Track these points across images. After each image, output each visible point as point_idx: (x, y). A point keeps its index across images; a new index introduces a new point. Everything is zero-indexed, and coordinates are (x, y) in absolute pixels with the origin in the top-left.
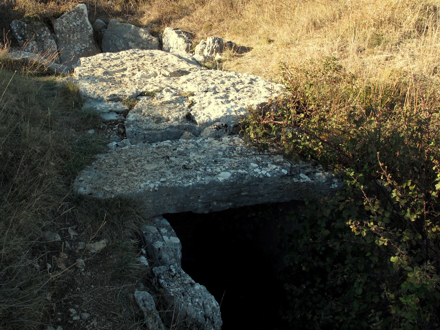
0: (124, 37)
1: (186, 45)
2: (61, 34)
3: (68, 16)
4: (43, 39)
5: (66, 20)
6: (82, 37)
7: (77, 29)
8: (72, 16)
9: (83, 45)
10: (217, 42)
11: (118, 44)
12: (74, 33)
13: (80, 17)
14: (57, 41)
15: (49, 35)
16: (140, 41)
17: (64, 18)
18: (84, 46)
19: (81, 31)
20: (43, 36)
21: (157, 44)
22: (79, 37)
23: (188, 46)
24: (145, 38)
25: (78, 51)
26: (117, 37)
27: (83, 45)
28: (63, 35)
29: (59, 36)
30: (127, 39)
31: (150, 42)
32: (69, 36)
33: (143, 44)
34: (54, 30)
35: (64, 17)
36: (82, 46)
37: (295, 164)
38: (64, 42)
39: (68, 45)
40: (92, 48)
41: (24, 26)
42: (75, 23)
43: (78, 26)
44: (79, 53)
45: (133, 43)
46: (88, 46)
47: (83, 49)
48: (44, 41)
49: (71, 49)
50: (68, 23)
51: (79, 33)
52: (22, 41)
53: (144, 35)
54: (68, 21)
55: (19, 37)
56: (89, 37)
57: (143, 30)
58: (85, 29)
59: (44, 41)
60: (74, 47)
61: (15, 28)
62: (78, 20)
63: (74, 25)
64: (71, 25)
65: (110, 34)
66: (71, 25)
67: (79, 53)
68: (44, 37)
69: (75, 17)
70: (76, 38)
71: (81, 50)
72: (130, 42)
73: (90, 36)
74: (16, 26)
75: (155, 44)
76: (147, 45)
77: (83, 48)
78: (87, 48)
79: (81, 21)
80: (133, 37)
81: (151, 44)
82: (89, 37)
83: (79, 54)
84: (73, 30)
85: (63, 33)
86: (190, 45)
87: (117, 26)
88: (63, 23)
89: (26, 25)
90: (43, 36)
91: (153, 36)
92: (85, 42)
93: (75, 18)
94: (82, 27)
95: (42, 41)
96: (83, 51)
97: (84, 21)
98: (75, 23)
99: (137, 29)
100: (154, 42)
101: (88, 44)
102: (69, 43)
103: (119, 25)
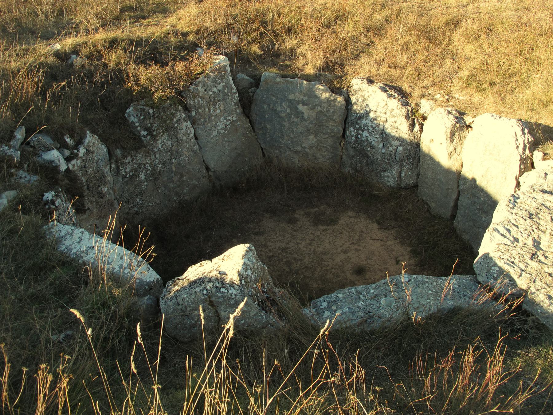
0: (290, 98)
1: (404, 110)
2: (197, 110)
3: (206, 80)
4: (176, 125)
5: (203, 86)
6: (226, 107)
7: (218, 97)
8: (211, 79)
9: (229, 118)
10: (528, 133)
11: (279, 109)
12: (215, 104)
13: (222, 77)
14: (193, 123)
15: (184, 115)
16: (317, 103)
17: (200, 85)
18: (230, 120)
19: (224, 99)
20: (175, 120)
21: (344, 105)
22: (222, 108)
23: (408, 111)
24: (326, 98)
25: (221, 129)
26: (277, 99)
27: (229, 118)
28: (200, 110)
29: (196, 113)
30: (295, 102)
31: (332, 103)
32: (209, 110)
33: (321, 106)
34: (188, 106)
35: (199, 82)
36: (227, 121)
37: (64, 87)
38: (202, 120)
39: (209, 123)
40: (240, 120)
41: (149, 113)
42: (215, 89)
43: (220, 91)
44: (224, 131)
45: (306, 107)
46: (234, 119)
47: (228, 125)
48: (177, 127)
49: (213, 128)
50: (205, 90)
51: (221, 103)
52: (149, 137)
53: (324, 93)
54: (205, 88)
55: (144, 133)
56: (235, 105)
57: (322, 87)
58: (229, 94)
59: (177, 127)
60: (216, 124)
61: (135, 120)
62: (220, 84)
63: (214, 92)
64: (211, 93)
65: (265, 96)
66: (211, 93)
67: (224, 131)
68: (177, 122)
69: (216, 80)
70: (218, 111)
71: (226, 126)
72: (301, 105)
73: (236, 104)
74: (137, 116)
75: (341, 106)
76: (327, 108)
77: (229, 123)
78: (233, 121)
79: (224, 84)
80: (305, 99)
81: (334, 106)
82: (235, 105)
83: (224, 133)
84: (213, 100)
85: (200, 108)
86: (410, 108)
87: (277, 83)
88: (199, 92)
89: (151, 111)
90: (175, 120)
91: (336, 93)
92: (230, 113)
93: (215, 82)
94: (226, 93)
95: (175, 128)
96: (229, 126)
97: (228, 83)
98: (215, 88)
99: (311, 86)
100: (339, 102)
101: (235, 115)
102: (210, 120)
103: (280, 82)
